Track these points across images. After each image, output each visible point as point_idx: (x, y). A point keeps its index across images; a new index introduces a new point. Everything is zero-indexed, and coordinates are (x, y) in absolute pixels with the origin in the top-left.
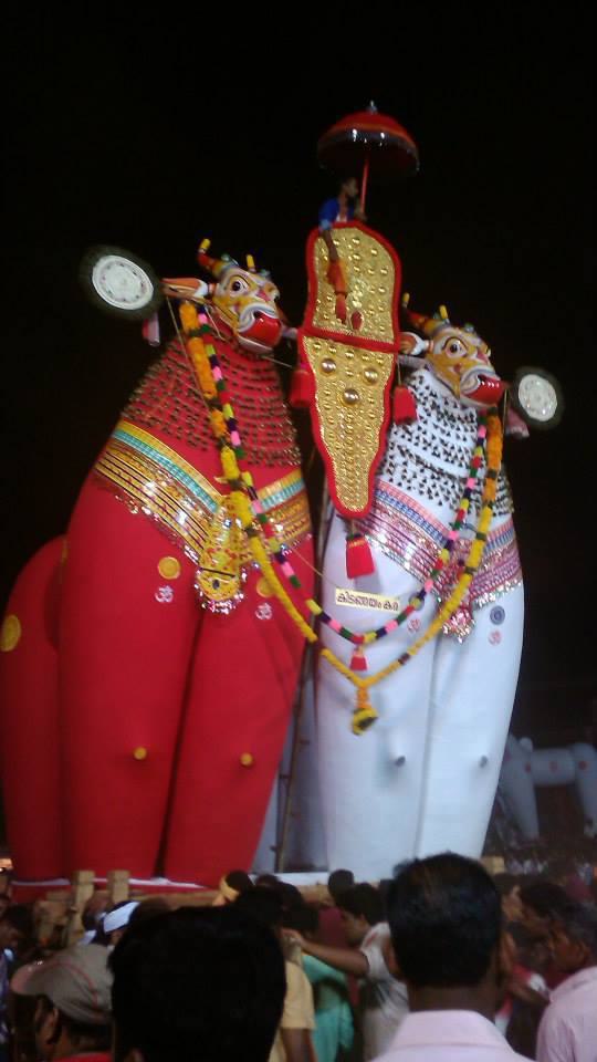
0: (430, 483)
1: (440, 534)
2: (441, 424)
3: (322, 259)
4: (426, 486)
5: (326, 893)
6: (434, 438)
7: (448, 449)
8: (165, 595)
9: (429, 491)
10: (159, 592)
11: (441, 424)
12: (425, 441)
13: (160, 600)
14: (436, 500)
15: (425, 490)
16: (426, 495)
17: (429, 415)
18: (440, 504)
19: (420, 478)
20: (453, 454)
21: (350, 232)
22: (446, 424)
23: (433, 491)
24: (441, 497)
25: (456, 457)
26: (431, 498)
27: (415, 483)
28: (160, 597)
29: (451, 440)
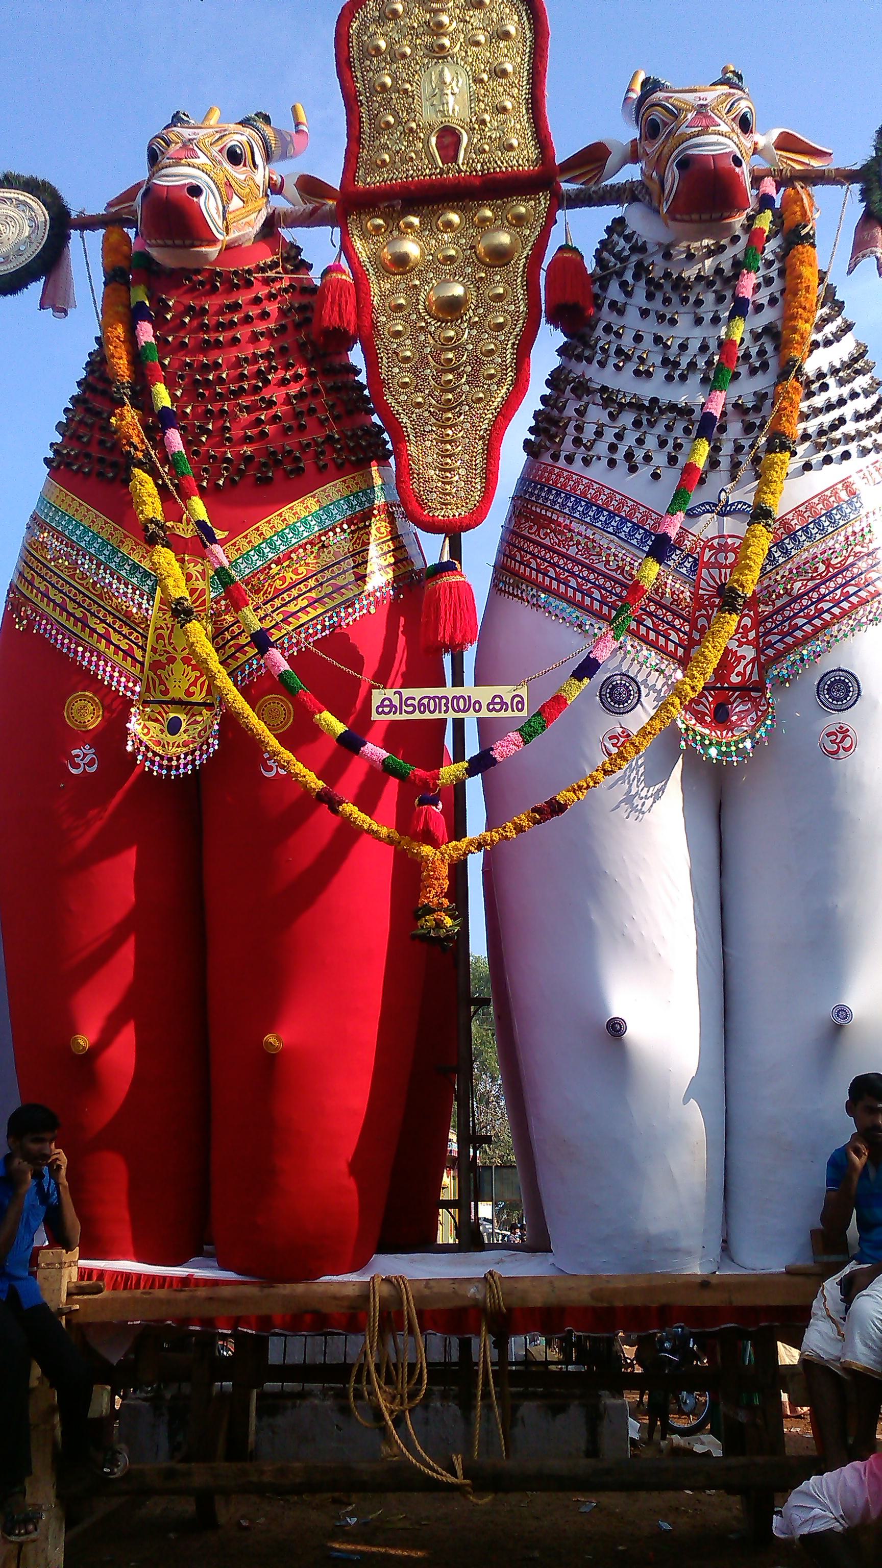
0: (630, 438)
1: (636, 527)
2: (657, 305)
3: (65, 1187)
4: (622, 449)
5: (160, 405)
6: (638, 338)
7: (672, 354)
8: (83, 760)
9: (629, 456)
10: (72, 758)
11: (657, 305)
12: (619, 352)
13: (74, 771)
14: (645, 471)
15: (619, 456)
16: (622, 466)
17: (629, 294)
18: (656, 476)
19: (609, 436)
20: (684, 362)
21: (158, 393)
22: (667, 301)
23: (639, 455)
24: (660, 459)
25: (692, 365)
26: (633, 469)
27: (602, 448)
28: (77, 766)
29: (674, 336)
